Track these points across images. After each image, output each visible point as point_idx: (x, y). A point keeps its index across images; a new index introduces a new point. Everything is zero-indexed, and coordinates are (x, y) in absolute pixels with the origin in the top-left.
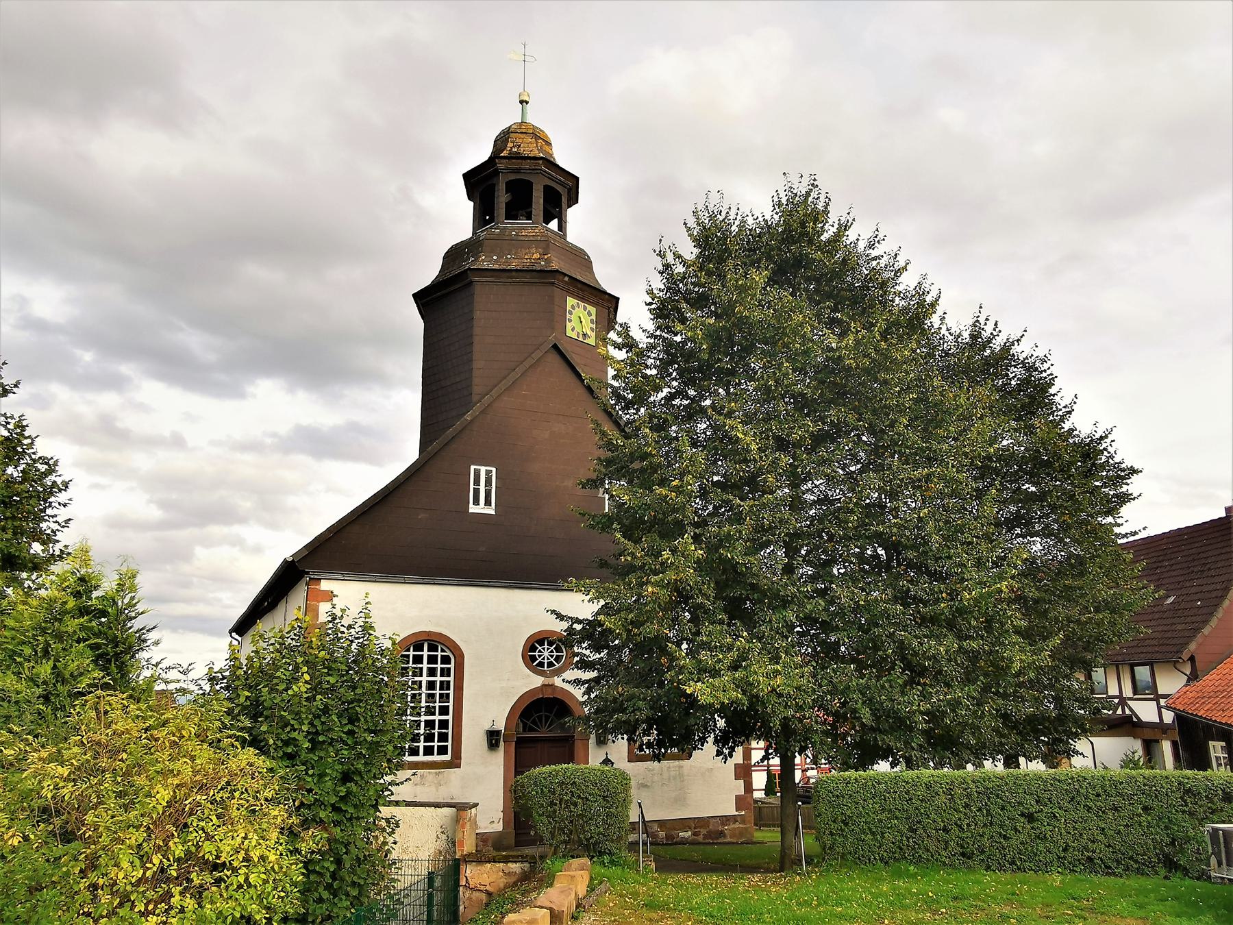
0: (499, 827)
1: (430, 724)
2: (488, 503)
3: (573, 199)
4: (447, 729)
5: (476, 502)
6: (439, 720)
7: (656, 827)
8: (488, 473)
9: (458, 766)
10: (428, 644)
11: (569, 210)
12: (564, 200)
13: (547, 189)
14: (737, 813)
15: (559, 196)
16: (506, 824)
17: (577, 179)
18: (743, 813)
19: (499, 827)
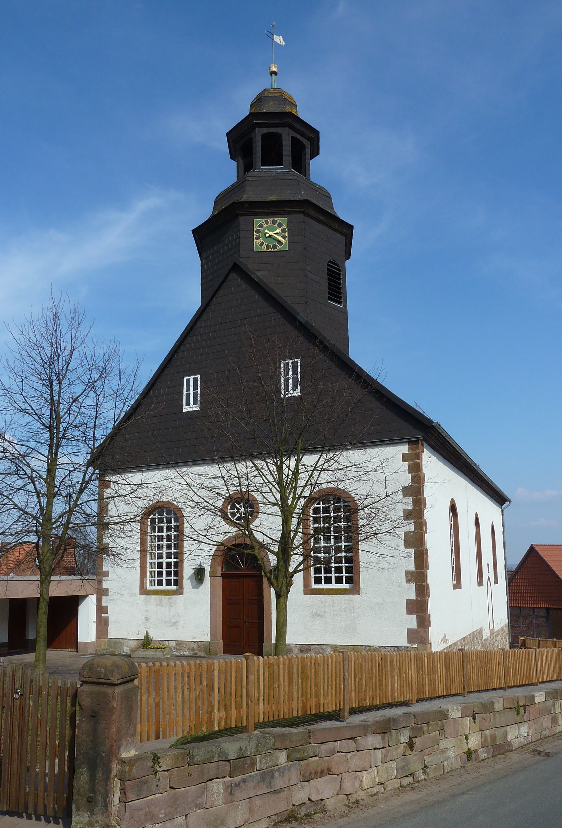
0: (208, 639)
1: (169, 565)
2: (195, 403)
3: (315, 152)
4: (315, 577)
5: (188, 404)
6: (324, 574)
7: (329, 650)
8: (195, 380)
9: (182, 594)
10: (166, 509)
11: (311, 161)
12: (308, 151)
13: (294, 140)
14: (409, 645)
15: (304, 147)
16: (213, 635)
17: (318, 133)
18: (416, 645)
19: (208, 639)
